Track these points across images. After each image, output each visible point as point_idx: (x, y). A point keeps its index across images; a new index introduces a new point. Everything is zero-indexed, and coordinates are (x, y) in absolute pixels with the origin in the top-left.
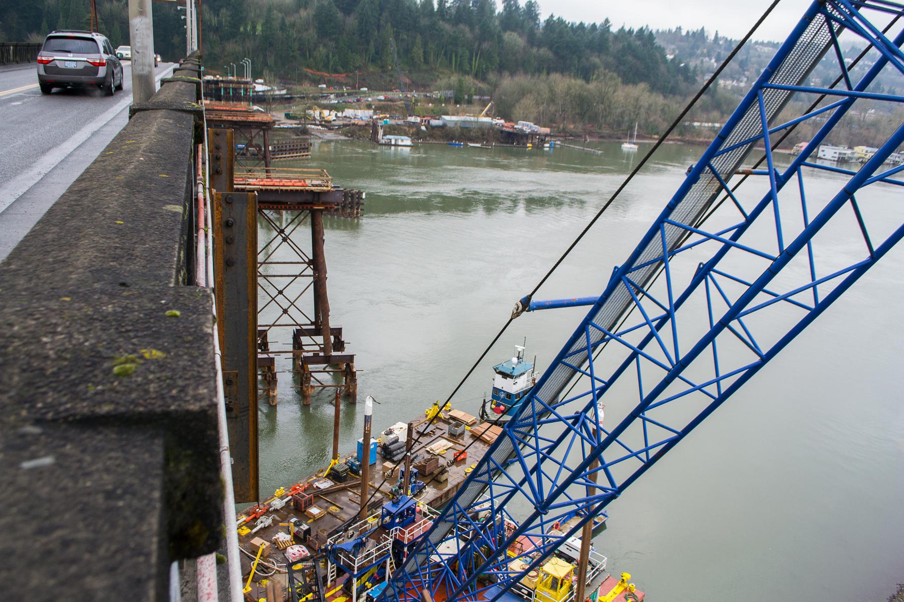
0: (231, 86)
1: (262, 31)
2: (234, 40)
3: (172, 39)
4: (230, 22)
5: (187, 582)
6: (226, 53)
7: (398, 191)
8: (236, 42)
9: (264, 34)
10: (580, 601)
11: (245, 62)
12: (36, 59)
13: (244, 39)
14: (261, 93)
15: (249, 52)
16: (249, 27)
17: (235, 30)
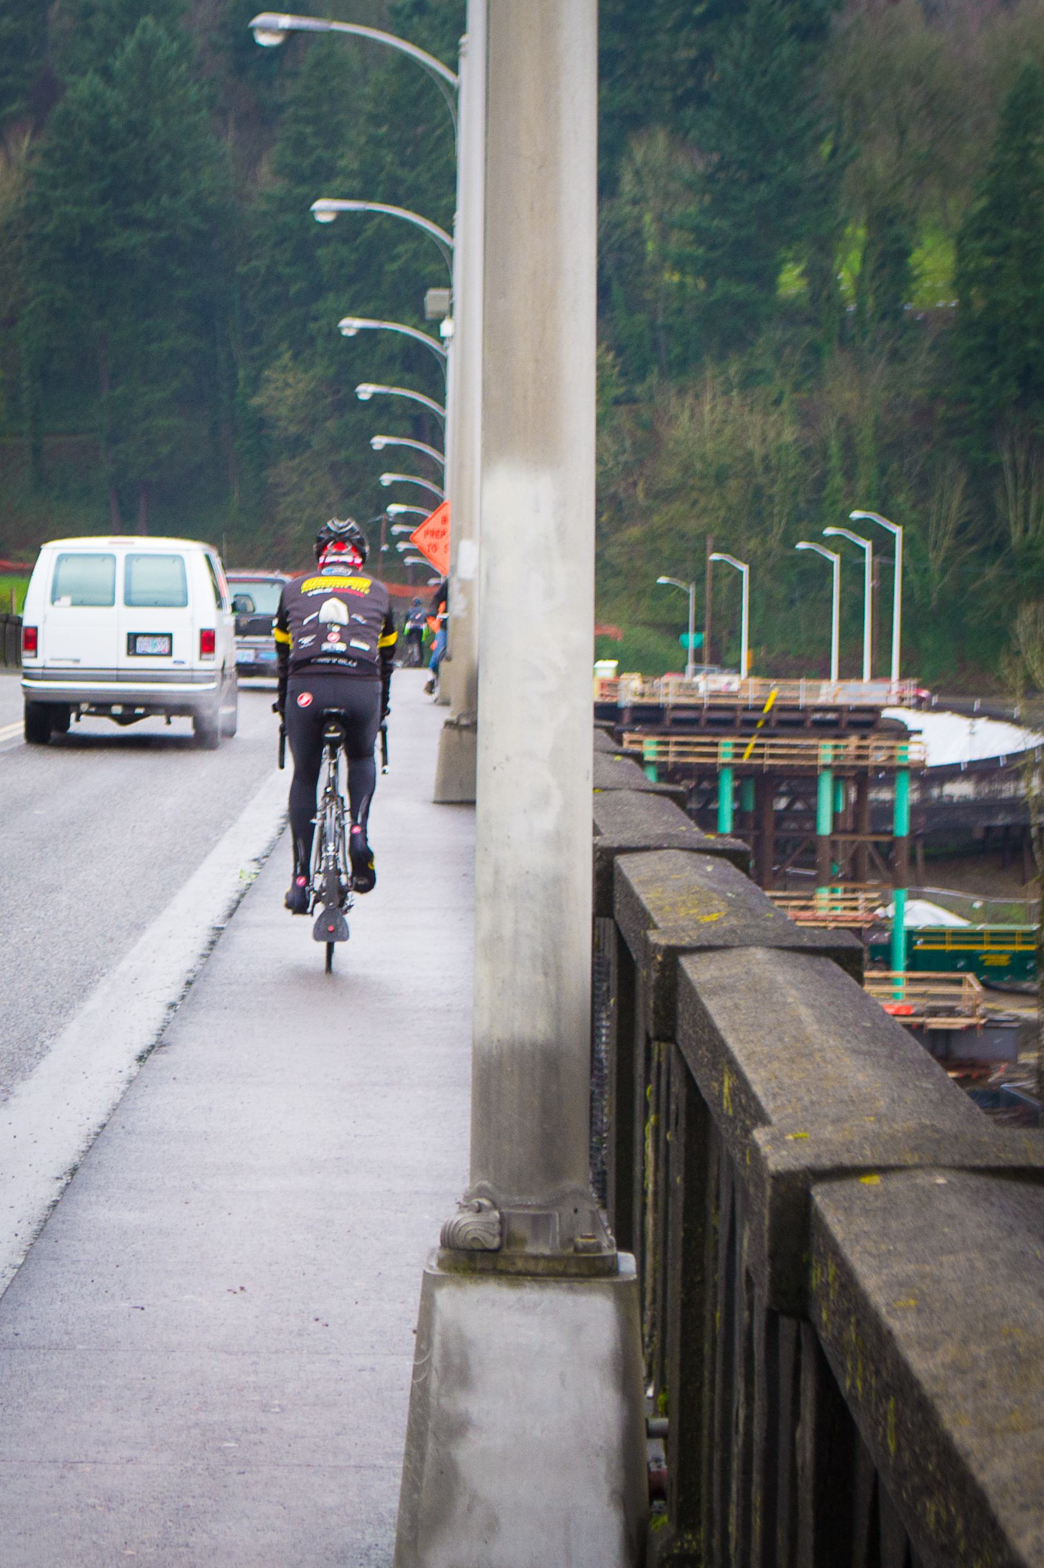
0: (726, 749)
1: (962, 281)
2: (734, 369)
3: (256, 383)
4: (702, 236)
5: (99, 1452)
6: (670, 473)
7: (957, 1023)
8: (750, 379)
9: (979, 305)
10: (782, 1560)
11: (835, 543)
12: (18, 662)
13: (815, 350)
14: (960, 790)
15: (848, 446)
16: (855, 258)
17: (739, 290)
